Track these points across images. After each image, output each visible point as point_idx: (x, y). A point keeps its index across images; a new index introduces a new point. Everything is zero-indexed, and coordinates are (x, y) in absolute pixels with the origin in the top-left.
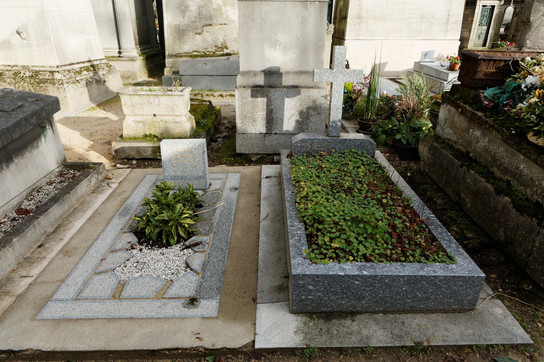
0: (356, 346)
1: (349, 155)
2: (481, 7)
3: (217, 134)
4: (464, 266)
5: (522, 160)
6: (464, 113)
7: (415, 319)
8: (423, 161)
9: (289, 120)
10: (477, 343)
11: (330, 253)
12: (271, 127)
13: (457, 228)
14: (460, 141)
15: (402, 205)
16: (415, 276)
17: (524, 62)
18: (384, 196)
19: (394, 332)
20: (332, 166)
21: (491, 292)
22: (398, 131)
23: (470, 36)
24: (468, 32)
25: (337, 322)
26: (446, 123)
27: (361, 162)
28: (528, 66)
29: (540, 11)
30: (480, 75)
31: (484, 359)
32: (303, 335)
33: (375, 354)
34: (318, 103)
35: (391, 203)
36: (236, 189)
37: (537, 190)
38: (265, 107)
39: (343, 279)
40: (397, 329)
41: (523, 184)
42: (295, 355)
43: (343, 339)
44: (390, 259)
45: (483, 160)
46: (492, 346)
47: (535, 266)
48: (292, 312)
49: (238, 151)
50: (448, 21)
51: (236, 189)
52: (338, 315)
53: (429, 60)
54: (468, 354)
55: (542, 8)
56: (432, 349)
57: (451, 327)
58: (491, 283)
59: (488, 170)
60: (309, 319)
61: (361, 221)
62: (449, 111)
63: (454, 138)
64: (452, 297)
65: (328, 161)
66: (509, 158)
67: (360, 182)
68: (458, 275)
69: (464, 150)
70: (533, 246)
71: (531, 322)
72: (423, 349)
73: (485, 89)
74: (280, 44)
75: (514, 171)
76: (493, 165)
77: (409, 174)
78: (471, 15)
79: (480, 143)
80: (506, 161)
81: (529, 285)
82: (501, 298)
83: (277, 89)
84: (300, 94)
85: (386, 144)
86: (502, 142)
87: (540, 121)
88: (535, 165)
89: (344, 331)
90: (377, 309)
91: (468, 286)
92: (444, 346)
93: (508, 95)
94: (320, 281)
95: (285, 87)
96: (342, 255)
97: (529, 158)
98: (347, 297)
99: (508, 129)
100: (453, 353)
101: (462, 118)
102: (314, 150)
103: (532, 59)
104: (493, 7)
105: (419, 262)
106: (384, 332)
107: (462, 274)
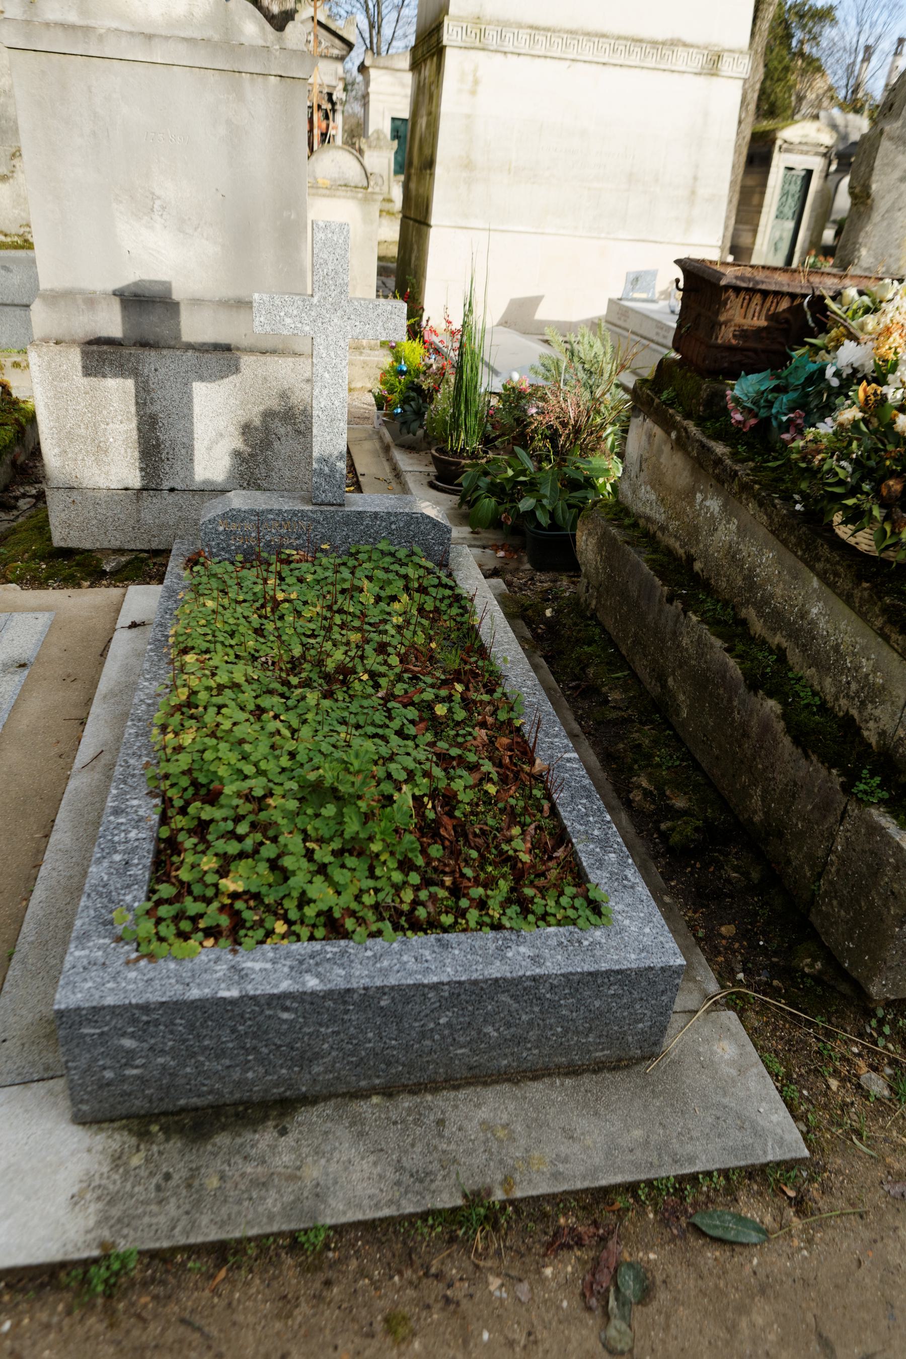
0: (275, 1228)
1: (370, 559)
2: (782, 171)
3: (22, 484)
4: (636, 930)
5: (815, 590)
6: (682, 444)
7: (478, 1106)
8: (586, 576)
9: (209, 449)
10: (651, 1176)
11: (213, 916)
12: (155, 468)
13: (650, 781)
14: (673, 525)
15: (490, 720)
16: (475, 982)
17: (841, 303)
18: (443, 693)
19: (406, 1163)
20: (311, 596)
21: (713, 987)
22: (532, 487)
23: (754, 243)
24: (750, 234)
25: (228, 1141)
26: (641, 470)
27: (401, 583)
28: (850, 313)
29: (895, 167)
30: (726, 335)
31: (667, 1226)
32: (100, 1205)
33: (334, 1250)
34: (294, 400)
35: (460, 715)
36: (23, 666)
37: (848, 683)
38: (133, 409)
39: (237, 1011)
40: (418, 1148)
41: (814, 661)
42: (59, 1288)
43: (236, 1208)
44: (408, 922)
45: (724, 585)
46: (693, 1178)
47: (832, 907)
48: (81, 1120)
49: (59, 538)
50: (693, 193)
51: (23, 666)
52: (237, 1115)
53: (644, 296)
54: (621, 1214)
55: (900, 158)
56: (517, 1211)
57: (582, 1123)
58: (719, 953)
59: (735, 614)
60: (134, 1141)
61: (335, 795)
62: (650, 436)
63: (659, 515)
64: (590, 1030)
65: (301, 580)
66: (785, 582)
67: (382, 649)
68: (604, 966)
69: (681, 551)
70: (830, 851)
71: (812, 1078)
72: (486, 1217)
73: (736, 377)
74: (163, 208)
75: (795, 622)
76: (748, 601)
77: (548, 613)
78: (758, 189)
79: (719, 533)
80: (779, 591)
81: (815, 960)
82: (736, 1003)
83: (165, 352)
84: (237, 370)
85: (496, 524)
86: (770, 535)
87: (862, 479)
88: (847, 610)
89: (243, 1175)
90: (363, 1083)
91: (636, 995)
92: (554, 1196)
93: (793, 395)
94: (157, 1023)
95: (190, 347)
96: (251, 916)
97: (832, 586)
98: (261, 1060)
99: (787, 498)
100: (580, 1214)
101: (678, 459)
102: (268, 544)
103: (861, 293)
104: (809, 173)
105: (497, 927)
106: (375, 1164)
107: (618, 962)
